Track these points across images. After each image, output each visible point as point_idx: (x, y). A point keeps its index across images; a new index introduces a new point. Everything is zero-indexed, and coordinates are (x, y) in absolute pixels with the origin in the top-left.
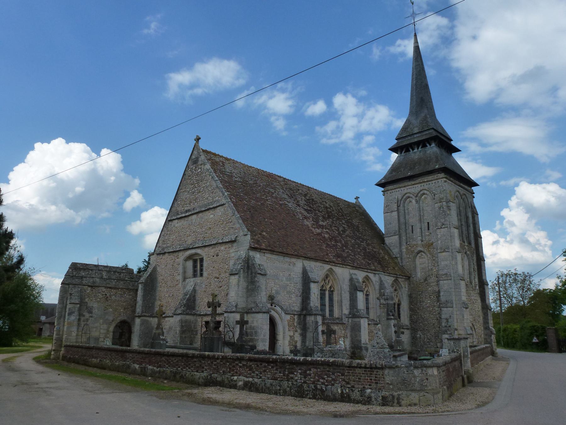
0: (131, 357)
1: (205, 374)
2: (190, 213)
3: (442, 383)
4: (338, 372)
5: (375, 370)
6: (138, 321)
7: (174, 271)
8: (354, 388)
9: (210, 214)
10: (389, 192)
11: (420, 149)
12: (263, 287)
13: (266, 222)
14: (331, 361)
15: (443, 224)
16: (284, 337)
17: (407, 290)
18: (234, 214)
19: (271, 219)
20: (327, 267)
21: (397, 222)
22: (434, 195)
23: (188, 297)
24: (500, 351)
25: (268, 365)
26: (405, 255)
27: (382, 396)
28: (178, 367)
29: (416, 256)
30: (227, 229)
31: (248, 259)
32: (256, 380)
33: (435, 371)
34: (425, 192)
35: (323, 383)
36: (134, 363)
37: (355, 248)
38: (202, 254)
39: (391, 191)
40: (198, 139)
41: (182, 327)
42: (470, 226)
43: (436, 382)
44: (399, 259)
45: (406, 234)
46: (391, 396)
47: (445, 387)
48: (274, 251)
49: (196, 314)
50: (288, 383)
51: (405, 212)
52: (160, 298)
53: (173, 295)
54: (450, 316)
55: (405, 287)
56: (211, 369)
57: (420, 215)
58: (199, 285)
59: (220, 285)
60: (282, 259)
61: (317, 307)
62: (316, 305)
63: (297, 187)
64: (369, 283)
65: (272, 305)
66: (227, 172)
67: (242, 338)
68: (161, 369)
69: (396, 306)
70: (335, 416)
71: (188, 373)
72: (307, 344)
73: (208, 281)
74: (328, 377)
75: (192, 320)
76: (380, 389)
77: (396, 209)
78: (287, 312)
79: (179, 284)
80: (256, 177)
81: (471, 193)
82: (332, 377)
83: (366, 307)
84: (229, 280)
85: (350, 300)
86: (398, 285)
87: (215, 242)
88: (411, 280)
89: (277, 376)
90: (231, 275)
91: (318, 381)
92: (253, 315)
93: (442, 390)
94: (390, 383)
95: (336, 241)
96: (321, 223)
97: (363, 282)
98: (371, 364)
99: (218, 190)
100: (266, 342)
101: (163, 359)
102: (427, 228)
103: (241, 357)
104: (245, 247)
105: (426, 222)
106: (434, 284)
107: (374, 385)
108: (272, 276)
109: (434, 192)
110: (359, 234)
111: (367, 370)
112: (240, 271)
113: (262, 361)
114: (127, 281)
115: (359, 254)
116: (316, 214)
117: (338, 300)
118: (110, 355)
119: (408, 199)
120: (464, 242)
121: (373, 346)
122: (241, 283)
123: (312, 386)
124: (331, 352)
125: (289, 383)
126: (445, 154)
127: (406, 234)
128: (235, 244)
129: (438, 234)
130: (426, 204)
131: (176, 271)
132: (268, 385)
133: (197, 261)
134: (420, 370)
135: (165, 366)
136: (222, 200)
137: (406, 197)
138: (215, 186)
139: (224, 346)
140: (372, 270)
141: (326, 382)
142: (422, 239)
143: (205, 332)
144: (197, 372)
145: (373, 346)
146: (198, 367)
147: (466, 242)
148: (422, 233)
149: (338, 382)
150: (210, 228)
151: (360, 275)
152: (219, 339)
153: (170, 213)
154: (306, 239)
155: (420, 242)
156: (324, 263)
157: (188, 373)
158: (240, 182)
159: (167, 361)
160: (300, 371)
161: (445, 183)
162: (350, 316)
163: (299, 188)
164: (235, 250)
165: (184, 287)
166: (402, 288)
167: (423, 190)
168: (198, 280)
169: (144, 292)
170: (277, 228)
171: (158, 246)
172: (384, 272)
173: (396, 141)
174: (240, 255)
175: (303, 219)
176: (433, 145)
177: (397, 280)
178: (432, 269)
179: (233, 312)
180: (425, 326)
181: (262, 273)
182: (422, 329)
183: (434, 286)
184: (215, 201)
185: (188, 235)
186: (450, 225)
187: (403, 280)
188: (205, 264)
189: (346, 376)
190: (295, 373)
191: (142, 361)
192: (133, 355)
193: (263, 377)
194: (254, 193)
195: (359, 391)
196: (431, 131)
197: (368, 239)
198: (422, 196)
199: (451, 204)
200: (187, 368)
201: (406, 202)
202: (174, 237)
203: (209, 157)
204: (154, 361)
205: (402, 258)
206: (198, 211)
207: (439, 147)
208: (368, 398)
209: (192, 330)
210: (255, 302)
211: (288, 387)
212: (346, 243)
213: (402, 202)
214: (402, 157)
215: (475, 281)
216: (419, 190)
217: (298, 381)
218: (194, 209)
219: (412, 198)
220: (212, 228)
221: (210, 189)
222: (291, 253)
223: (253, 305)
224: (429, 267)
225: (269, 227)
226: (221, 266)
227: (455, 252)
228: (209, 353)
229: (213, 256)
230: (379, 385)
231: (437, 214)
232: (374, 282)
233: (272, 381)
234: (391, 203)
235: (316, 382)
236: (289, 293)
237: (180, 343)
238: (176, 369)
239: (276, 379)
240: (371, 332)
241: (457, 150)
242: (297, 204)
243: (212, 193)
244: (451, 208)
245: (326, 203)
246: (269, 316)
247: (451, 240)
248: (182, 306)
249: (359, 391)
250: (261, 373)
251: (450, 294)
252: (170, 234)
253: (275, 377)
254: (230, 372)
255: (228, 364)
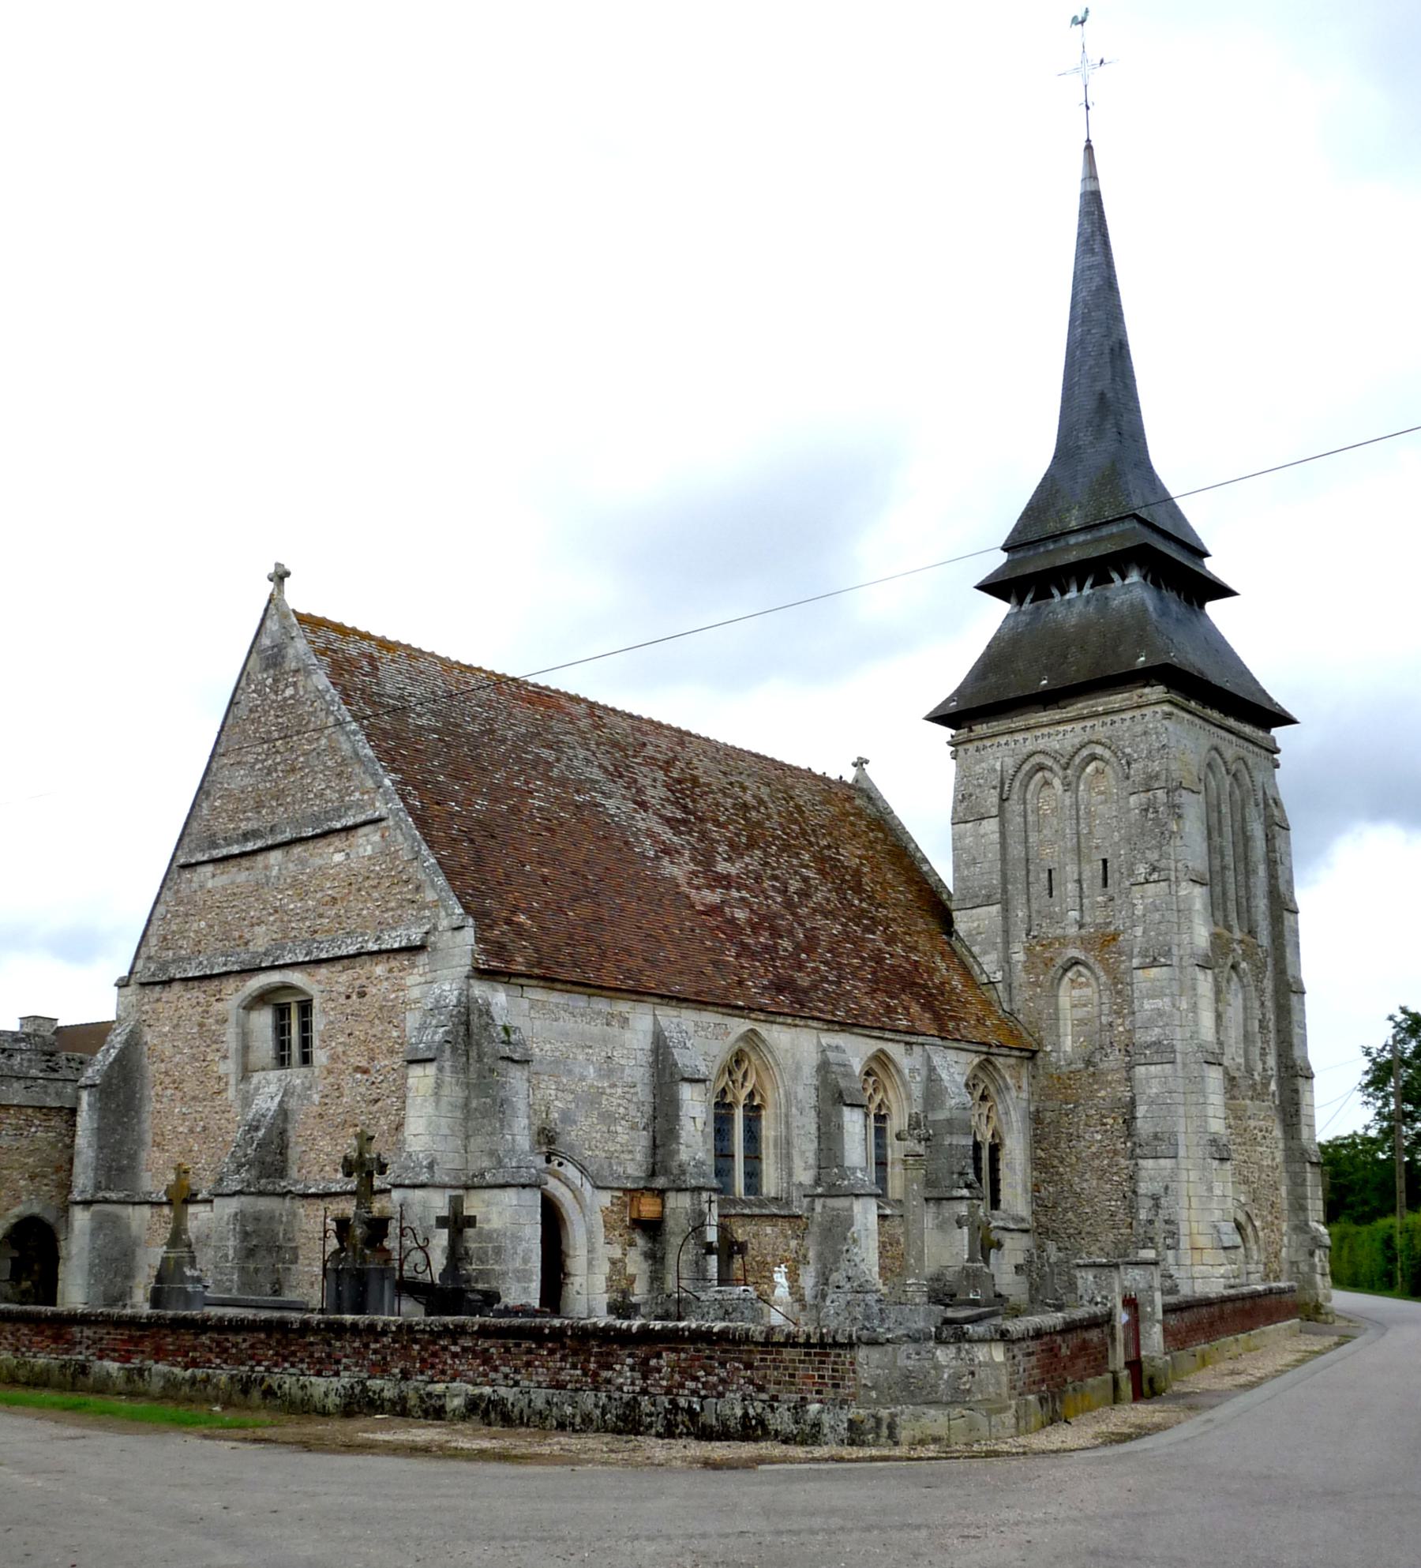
0: (88, 1338)
1: (345, 1380)
2: (260, 844)
3: (1020, 1384)
4: (733, 1359)
5: (833, 1352)
6: (81, 1218)
7: (208, 1046)
8: (778, 1401)
9: (332, 850)
10: (971, 747)
11: (1087, 591)
12: (521, 1104)
13: (527, 875)
14: (715, 1330)
15: (1154, 869)
16: (590, 1263)
17: (1024, 1095)
18: (418, 852)
19: (542, 864)
20: (739, 1026)
21: (999, 857)
22: (1129, 764)
23: (261, 1133)
24: (1342, 1300)
25: (540, 1346)
26: (1020, 976)
27: (850, 1421)
28: (254, 1363)
29: (1061, 979)
30: (393, 904)
31: (468, 1009)
32: (503, 1391)
33: (998, 1354)
34: (1098, 750)
35: (694, 1392)
36: (100, 1358)
37: (840, 955)
38: (306, 988)
39: (979, 744)
40: (280, 576)
41: (246, 1235)
42: (1255, 872)
43: (998, 1383)
44: (1000, 986)
45: (1028, 900)
46: (872, 1419)
47: (1031, 1397)
48: (554, 980)
49: (290, 1192)
50: (596, 1395)
51: (1026, 822)
52: (158, 1139)
53: (205, 1129)
54: (1167, 1188)
55: (1020, 1087)
56: (362, 1366)
57: (1078, 833)
58: (299, 1096)
59: (375, 1096)
60: (582, 1004)
61: (703, 1163)
62: (700, 1155)
63: (638, 735)
64: (890, 1076)
65: (548, 1161)
66: (390, 697)
67: (456, 1268)
68: (200, 1373)
69: (985, 1154)
70: (709, 1464)
71: (287, 1380)
72: (670, 1283)
73: (331, 1079)
74: (708, 1374)
75: (277, 1214)
76: (844, 1402)
77: (994, 811)
78: (600, 1184)
79: (225, 1090)
80: (491, 707)
81: (1267, 750)
82: (718, 1375)
83: (877, 1158)
84: (405, 1077)
85: (819, 1137)
86: (993, 1080)
87: (352, 950)
88: (1039, 1062)
89: (564, 1376)
90: (411, 1062)
91: (682, 1386)
92: (487, 1194)
93: (1017, 1404)
94: (870, 1384)
95: (775, 933)
96: (722, 867)
97: (868, 1074)
98: (822, 1335)
99: (358, 769)
100: (531, 1281)
101: (205, 1339)
102: (1100, 881)
103: (456, 1326)
104: (459, 969)
105: (1098, 857)
106: (1117, 1076)
107: (829, 1393)
108: (551, 1063)
109: (1128, 750)
110: (861, 901)
111: (813, 1351)
112: (440, 1049)
113: (519, 1333)
114: (35, 1079)
115: (854, 976)
116: (704, 836)
117: (776, 1137)
118: (12, 1334)
119: (1040, 774)
120: (1229, 928)
121: (838, 1287)
122: (445, 1091)
123: (665, 1401)
124: (721, 1306)
125: (599, 1394)
126: (1174, 604)
127: (1028, 900)
128: (422, 959)
129: (1135, 901)
130: (1100, 793)
131: (215, 1046)
132: (539, 1404)
133: (289, 1009)
134: (954, 1351)
135: (210, 1361)
136: (373, 804)
137: (1033, 766)
138: (349, 753)
139: (399, 1296)
140: (899, 1031)
141: (704, 1388)
142: (1082, 917)
143: (336, 1253)
144: (319, 1374)
145: (838, 1287)
146: (320, 1361)
147: (1236, 930)
148: (1081, 898)
149: (735, 1387)
150: (334, 899)
151: (856, 1051)
152: (384, 1273)
153: (186, 840)
154: (666, 928)
155: (1073, 931)
156: (729, 1015)
157: (288, 1379)
158: (435, 731)
159: (218, 1344)
160: (629, 1361)
161: (1166, 722)
162: (820, 1190)
163: (645, 739)
164: (423, 980)
165: (246, 1101)
166: (1008, 1088)
167: (1091, 742)
168: (296, 1075)
169: (102, 1118)
170: (566, 895)
171: (143, 955)
172: (943, 1038)
173: (1003, 557)
174: (440, 995)
175: (657, 857)
176: (1134, 577)
177: (991, 1063)
178: (1111, 1024)
179: (423, 1186)
180: (1083, 1222)
181: (516, 1057)
182: (1072, 1231)
183: (1119, 1082)
184: (349, 808)
185: (254, 920)
186: (1176, 870)
187: (1012, 1061)
188: (318, 1023)
189: (757, 1368)
190: (618, 1367)
191: (128, 1351)
192: (95, 1333)
193: (527, 1383)
194: (484, 769)
195: (789, 1409)
196: (1128, 525)
197: (894, 920)
198: (1088, 764)
199: (1185, 797)
200: (287, 1365)
201: (1031, 787)
202: (203, 924)
203: (320, 643)
204: (171, 1347)
205: (1010, 986)
206: (287, 835)
207: (1156, 584)
208: (814, 1425)
209: (280, 1248)
210: (492, 1153)
211: (596, 1406)
212: (812, 939)
213: (1017, 784)
214: (1024, 618)
215: (1264, 1063)
216: (1077, 741)
217: (625, 1389)
218: (272, 830)
219: (1051, 770)
220: (342, 899)
221: (329, 763)
222: (613, 984)
223: (486, 1163)
224: (1103, 1018)
225: (539, 895)
226: (377, 1030)
227: (1192, 965)
228: (357, 1317)
229: (348, 997)
230: (841, 1390)
231: (1133, 831)
232: (907, 1071)
233: (551, 1391)
234: (980, 786)
235: (675, 1390)
236: (608, 1118)
237: (239, 1289)
238: (247, 1368)
239: (560, 1386)
240: (891, 1245)
241: (1222, 591)
242: (635, 802)
243: (340, 775)
244: (1184, 811)
245: (744, 789)
246: (539, 1196)
247: (1179, 924)
248: (241, 1165)
249: (789, 1409)
250: (517, 1371)
251: (1170, 1111)
252: (187, 915)
253: (557, 1381)
254: (422, 1373)
255: (417, 1347)
